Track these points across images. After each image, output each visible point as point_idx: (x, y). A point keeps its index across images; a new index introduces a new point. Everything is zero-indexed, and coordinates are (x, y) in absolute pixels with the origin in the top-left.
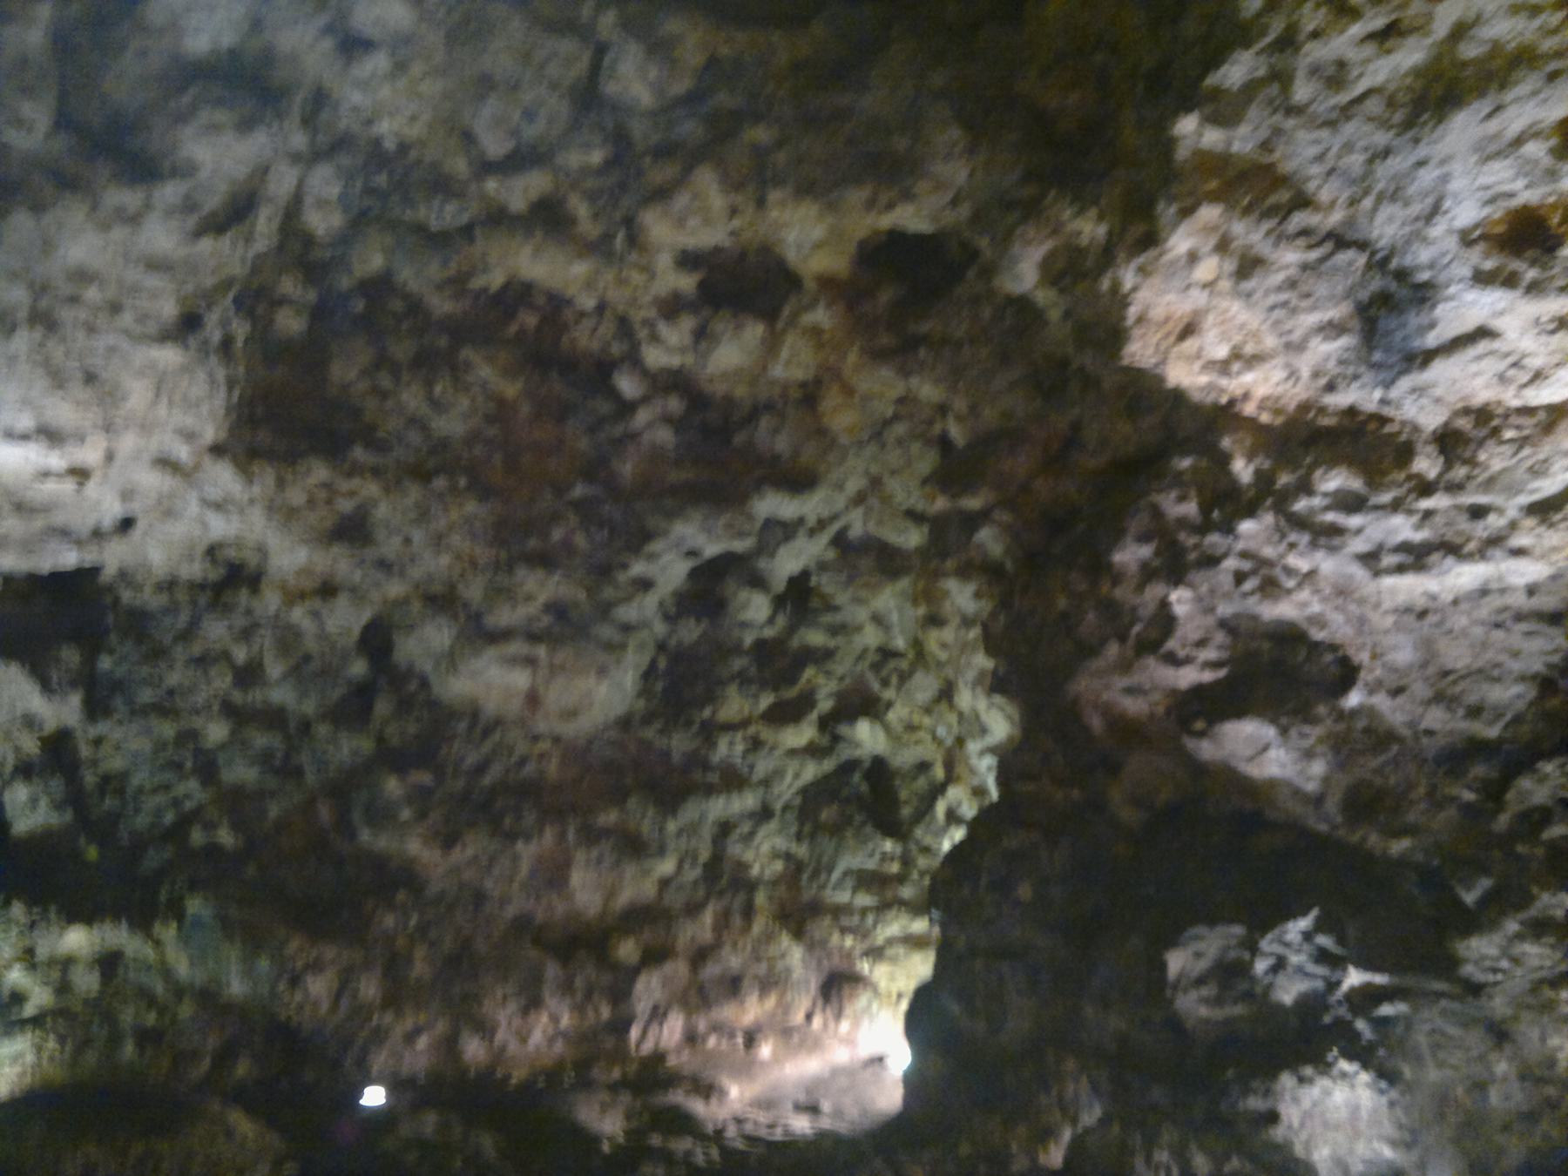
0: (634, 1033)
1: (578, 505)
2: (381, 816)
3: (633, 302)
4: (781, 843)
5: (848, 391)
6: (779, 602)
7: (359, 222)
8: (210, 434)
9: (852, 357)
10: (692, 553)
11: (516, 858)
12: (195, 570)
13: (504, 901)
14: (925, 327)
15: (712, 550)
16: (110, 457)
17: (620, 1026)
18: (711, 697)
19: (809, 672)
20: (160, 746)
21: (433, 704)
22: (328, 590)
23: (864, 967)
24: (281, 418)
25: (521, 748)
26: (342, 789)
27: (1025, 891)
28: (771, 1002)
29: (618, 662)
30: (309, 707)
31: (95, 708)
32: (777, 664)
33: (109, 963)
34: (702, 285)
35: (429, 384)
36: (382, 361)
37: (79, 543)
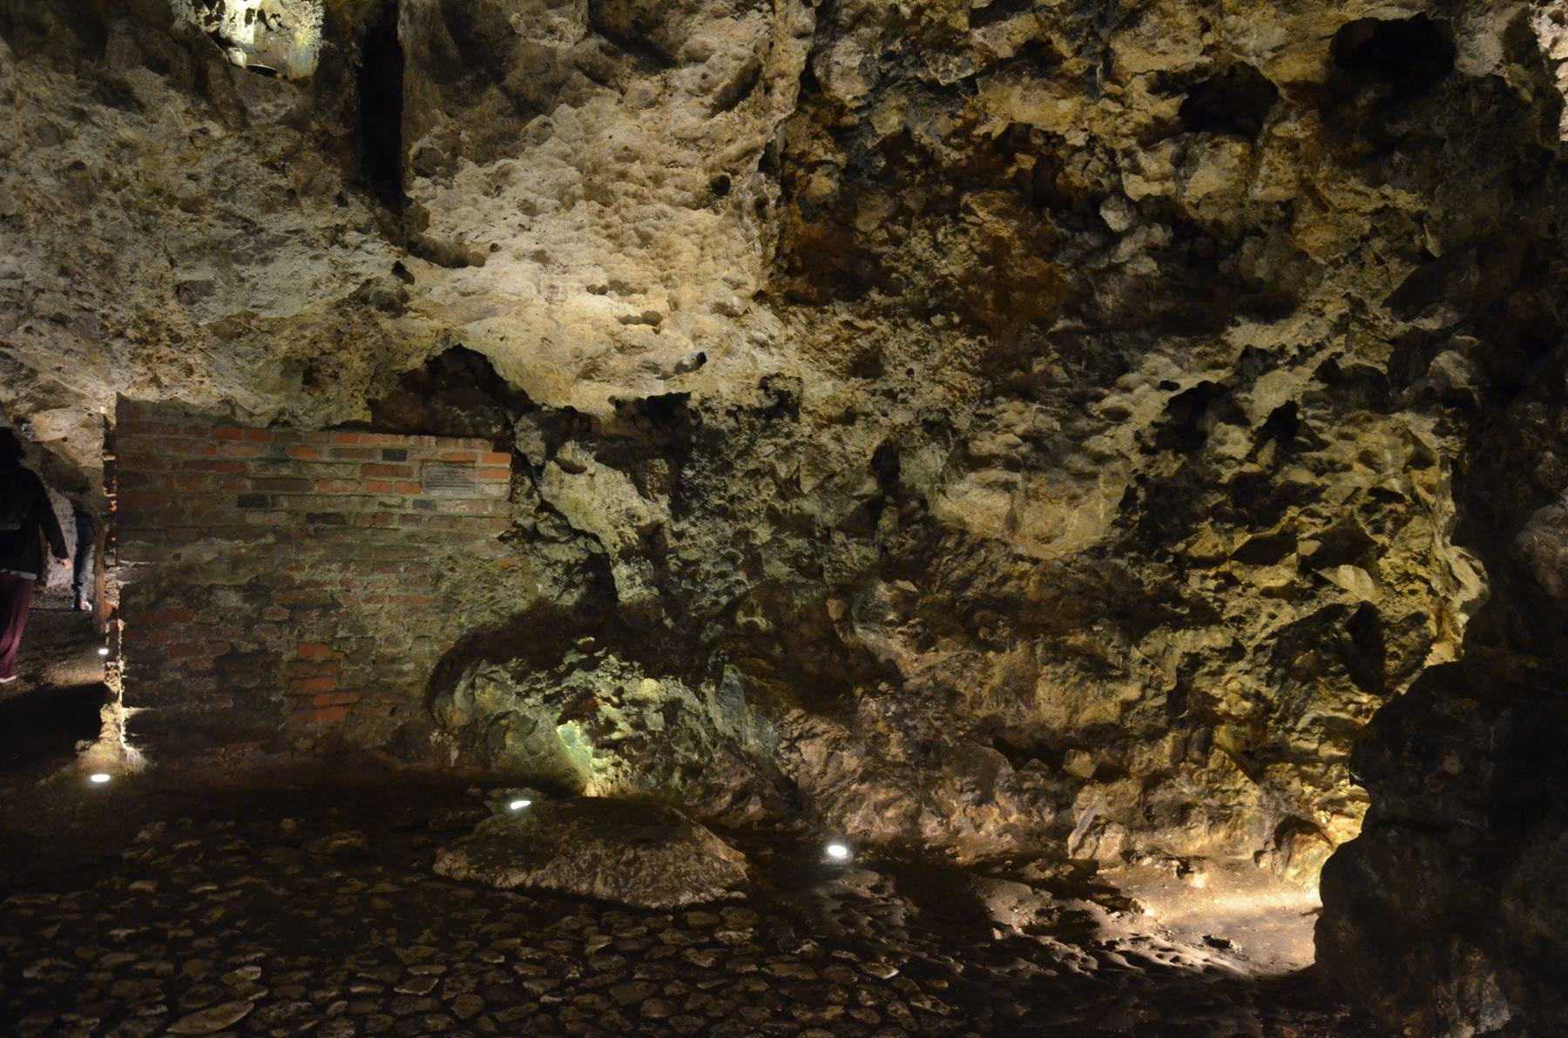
0: (1073, 840)
1: (1056, 338)
2: (872, 617)
3: (1115, 133)
4: (1250, 683)
5: (1322, 206)
6: (1260, 438)
7: (881, 84)
8: (752, 286)
9: (1324, 170)
10: (1168, 385)
11: (988, 665)
12: (753, 399)
13: (977, 702)
14: (1403, 127)
15: (1188, 382)
16: (675, 305)
17: (1061, 831)
18: (1186, 533)
19: (1293, 511)
20: (722, 542)
21: (929, 521)
22: (849, 417)
23: (1321, 817)
24: (816, 268)
25: (1004, 567)
26: (851, 589)
27: (1452, 765)
28: (1220, 835)
29: (1088, 491)
30: (829, 518)
31: (679, 509)
32: (1256, 501)
33: (671, 709)
34: (1183, 109)
35: (933, 229)
36: (902, 213)
37: (665, 377)
